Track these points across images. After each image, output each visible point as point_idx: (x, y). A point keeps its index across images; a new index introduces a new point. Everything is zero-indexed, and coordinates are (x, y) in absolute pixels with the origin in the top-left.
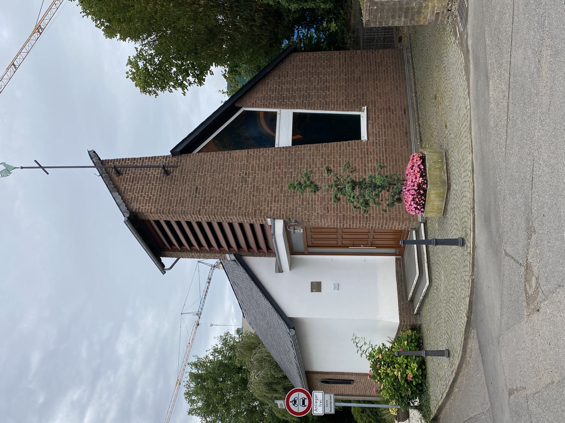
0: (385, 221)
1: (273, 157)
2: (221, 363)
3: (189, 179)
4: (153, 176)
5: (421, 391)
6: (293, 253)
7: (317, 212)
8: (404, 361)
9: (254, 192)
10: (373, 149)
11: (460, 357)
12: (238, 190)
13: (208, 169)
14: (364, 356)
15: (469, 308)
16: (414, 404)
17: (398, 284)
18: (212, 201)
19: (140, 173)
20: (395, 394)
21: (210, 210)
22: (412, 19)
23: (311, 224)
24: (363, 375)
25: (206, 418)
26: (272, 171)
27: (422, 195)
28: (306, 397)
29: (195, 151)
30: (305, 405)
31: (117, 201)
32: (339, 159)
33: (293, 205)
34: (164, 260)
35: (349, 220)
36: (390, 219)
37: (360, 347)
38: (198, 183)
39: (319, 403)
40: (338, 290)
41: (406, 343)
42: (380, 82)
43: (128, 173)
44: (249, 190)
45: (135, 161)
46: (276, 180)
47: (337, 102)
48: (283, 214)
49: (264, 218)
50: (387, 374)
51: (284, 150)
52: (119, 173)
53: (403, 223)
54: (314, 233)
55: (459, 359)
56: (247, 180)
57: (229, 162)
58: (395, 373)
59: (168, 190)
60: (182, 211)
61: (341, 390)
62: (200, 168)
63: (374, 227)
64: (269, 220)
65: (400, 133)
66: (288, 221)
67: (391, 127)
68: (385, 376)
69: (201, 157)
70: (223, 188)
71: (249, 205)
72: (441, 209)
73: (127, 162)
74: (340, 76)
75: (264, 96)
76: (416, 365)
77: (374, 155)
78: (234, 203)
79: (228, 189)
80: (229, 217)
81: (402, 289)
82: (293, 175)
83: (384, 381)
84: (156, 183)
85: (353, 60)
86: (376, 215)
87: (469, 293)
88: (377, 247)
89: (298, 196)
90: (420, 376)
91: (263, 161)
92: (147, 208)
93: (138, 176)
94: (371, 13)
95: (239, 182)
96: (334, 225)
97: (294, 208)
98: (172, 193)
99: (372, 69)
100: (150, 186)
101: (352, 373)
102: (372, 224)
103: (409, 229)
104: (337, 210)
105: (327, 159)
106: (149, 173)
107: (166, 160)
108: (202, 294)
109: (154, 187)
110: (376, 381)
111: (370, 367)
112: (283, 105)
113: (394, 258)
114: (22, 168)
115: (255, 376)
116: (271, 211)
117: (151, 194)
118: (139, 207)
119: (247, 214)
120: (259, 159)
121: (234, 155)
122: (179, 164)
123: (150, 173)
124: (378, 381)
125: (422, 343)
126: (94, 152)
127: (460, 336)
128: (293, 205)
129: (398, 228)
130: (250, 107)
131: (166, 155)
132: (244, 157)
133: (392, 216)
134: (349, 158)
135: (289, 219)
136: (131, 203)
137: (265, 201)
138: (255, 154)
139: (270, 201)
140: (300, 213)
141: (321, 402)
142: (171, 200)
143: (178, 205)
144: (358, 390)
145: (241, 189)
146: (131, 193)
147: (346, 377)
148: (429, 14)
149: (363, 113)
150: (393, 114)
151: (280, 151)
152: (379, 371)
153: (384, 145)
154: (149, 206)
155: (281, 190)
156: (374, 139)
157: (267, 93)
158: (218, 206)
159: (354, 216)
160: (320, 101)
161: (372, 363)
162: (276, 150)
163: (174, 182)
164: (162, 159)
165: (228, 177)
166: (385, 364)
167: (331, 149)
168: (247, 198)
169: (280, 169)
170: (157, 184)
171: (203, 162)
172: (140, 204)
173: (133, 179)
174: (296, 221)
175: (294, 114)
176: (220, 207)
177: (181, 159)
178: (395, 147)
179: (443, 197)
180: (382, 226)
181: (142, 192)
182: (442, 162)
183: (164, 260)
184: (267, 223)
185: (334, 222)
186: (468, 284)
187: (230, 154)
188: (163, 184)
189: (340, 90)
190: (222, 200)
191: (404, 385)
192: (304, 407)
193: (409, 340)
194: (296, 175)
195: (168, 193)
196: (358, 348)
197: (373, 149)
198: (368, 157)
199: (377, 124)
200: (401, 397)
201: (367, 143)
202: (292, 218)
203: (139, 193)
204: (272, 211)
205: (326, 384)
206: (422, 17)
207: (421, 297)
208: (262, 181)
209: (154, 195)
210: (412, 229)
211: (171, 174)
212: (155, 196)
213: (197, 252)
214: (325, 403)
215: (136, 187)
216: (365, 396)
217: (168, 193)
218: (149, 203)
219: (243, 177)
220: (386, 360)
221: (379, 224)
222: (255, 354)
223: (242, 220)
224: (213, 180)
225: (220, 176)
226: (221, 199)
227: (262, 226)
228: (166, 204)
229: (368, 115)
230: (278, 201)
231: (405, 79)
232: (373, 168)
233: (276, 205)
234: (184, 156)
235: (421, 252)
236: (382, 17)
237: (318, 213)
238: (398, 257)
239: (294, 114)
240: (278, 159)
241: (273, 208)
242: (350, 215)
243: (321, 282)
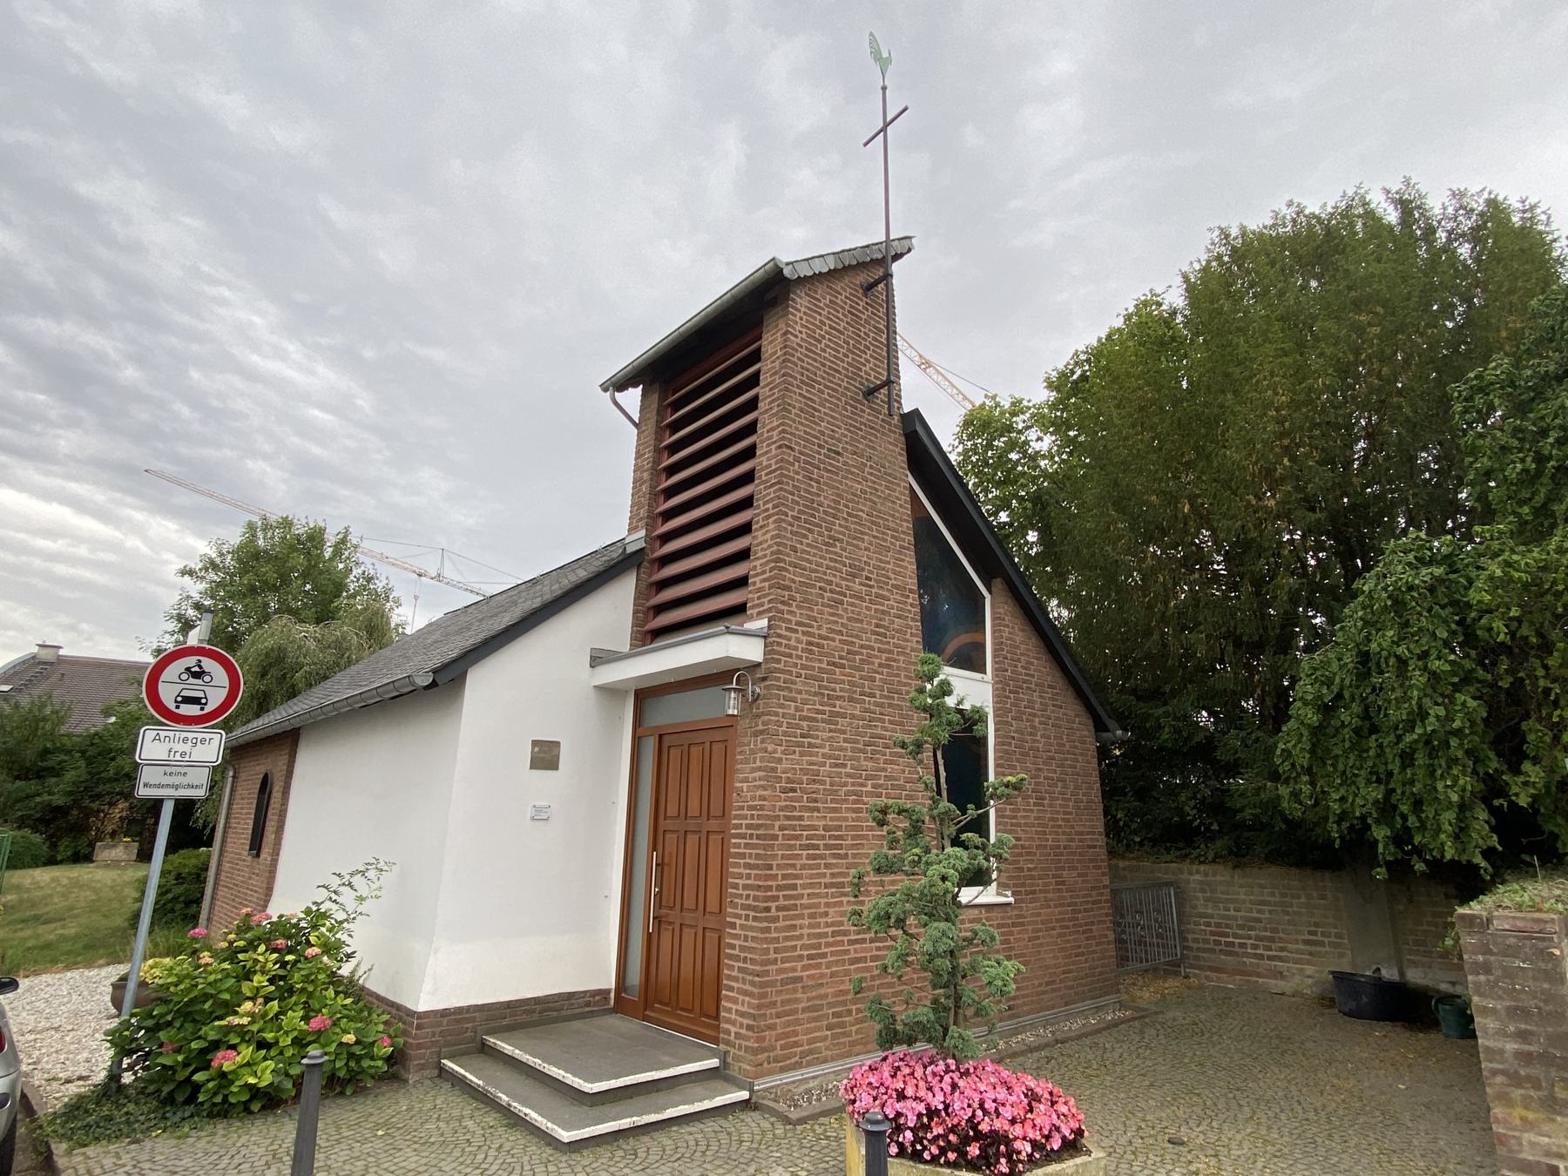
0: (758, 968)
2: (340, 587)
5: (170, 1100)
6: (640, 696)
8: (287, 1033)
12: (836, 553)
13: (876, 490)
14: (322, 895)
16: (126, 1070)
17: (536, 1000)
20: (171, 1007)
22: (1516, 1080)
23: (746, 740)
24: (268, 883)
25: (233, 553)
26: (876, 645)
27: (962, 1154)
28: (208, 709)
30: (182, 705)
33: (800, 692)
35: (763, 852)
36: (762, 985)
37: (350, 883)
39: (181, 747)
40: (533, 819)
41: (350, 1038)
42: (1060, 935)
44: (833, 579)
46: (856, 653)
48: (779, 661)
49: (769, 610)
50: (247, 975)
52: (869, 288)
53: (749, 1028)
54: (685, 753)
56: (857, 580)
57: (892, 543)
58: (248, 1006)
60: (789, 405)
61: (239, 823)
62: (880, 471)
64: (763, 623)
66: (758, 676)
68: (244, 966)
71: (802, 575)
75: (1018, 647)
76: (267, 1079)
79: (837, 528)
80: (771, 520)
81: (521, 1015)
82: (867, 699)
83: (226, 965)
86: (775, 938)
89: (821, 708)
90: (225, 1097)
94: (1525, 938)
97: (793, 695)
98: (828, 393)
99: (1080, 915)
101: (278, 855)
102: (743, 927)
104: (788, 818)
105: (904, 793)
108: (473, 585)
110: (232, 936)
111: (281, 916)
113: (610, 982)
114: (884, 89)
115: (307, 632)
116: (787, 629)
117: (826, 346)
118: (800, 311)
119: (782, 565)
120: (899, 617)
124: (231, 943)
125: (342, 1094)
126: (909, 250)
128: (800, 692)
129: (729, 1010)
130: (993, 613)
133: (769, 990)
135: (764, 679)
136: (808, 295)
137: (809, 617)
140: (780, 710)
141: (183, 754)
142: (814, 387)
144: (233, 868)
146: (828, 302)
147: (269, 837)
148: (1546, 1140)
149: (995, 893)
152: (262, 948)
155: (834, 664)
159: (771, 869)
161: (294, 921)
163: (851, 406)
165: (862, 533)
166: (284, 964)
169: (880, 665)
171: (892, 483)
173: (857, 316)
174: (756, 698)
177: (895, 432)
180: (736, 958)
184: (751, 618)
185: (751, 808)
187: (908, 549)
190: (814, 509)
191: (200, 1038)
192: (176, 701)
193: (357, 1050)
196: (348, 877)
200: (157, 1024)
202: (767, 687)
204: (787, 633)
205: (258, 786)
206: (1531, 1116)
207: (504, 1097)
209: (822, 350)
210: (724, 1057)
213: (654, 462)
214: (179, 769)
216: (216, 884)
218: (809, 336)
219: (863, 569)
220: (300, 969)
221: (742, 949)
222: (357, 634)
223: (760, 554)
224: (855, 495)
225: (864, 516)
227: (739, 610)
229: (996, 909)
231: (1067, 1004)
233: (800, 646)
235: (657, 1091)
237: (780, 761)
238: (612, 995)
240: (901, 664)
241: (793, 635)
242: (774, 857)
243: (557, 769)
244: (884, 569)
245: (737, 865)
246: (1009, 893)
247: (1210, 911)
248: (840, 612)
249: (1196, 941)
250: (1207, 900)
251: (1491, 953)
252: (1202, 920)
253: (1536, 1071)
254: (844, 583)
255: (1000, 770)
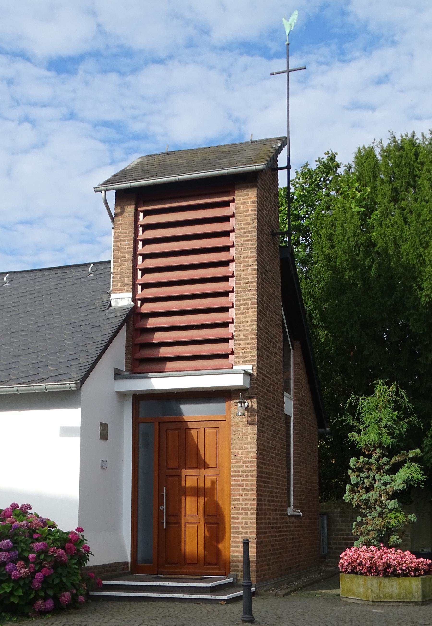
247: (344, 527)
249: (335, 544)
250: (343, 522)
252: (339, 533)
255: (296, 447)
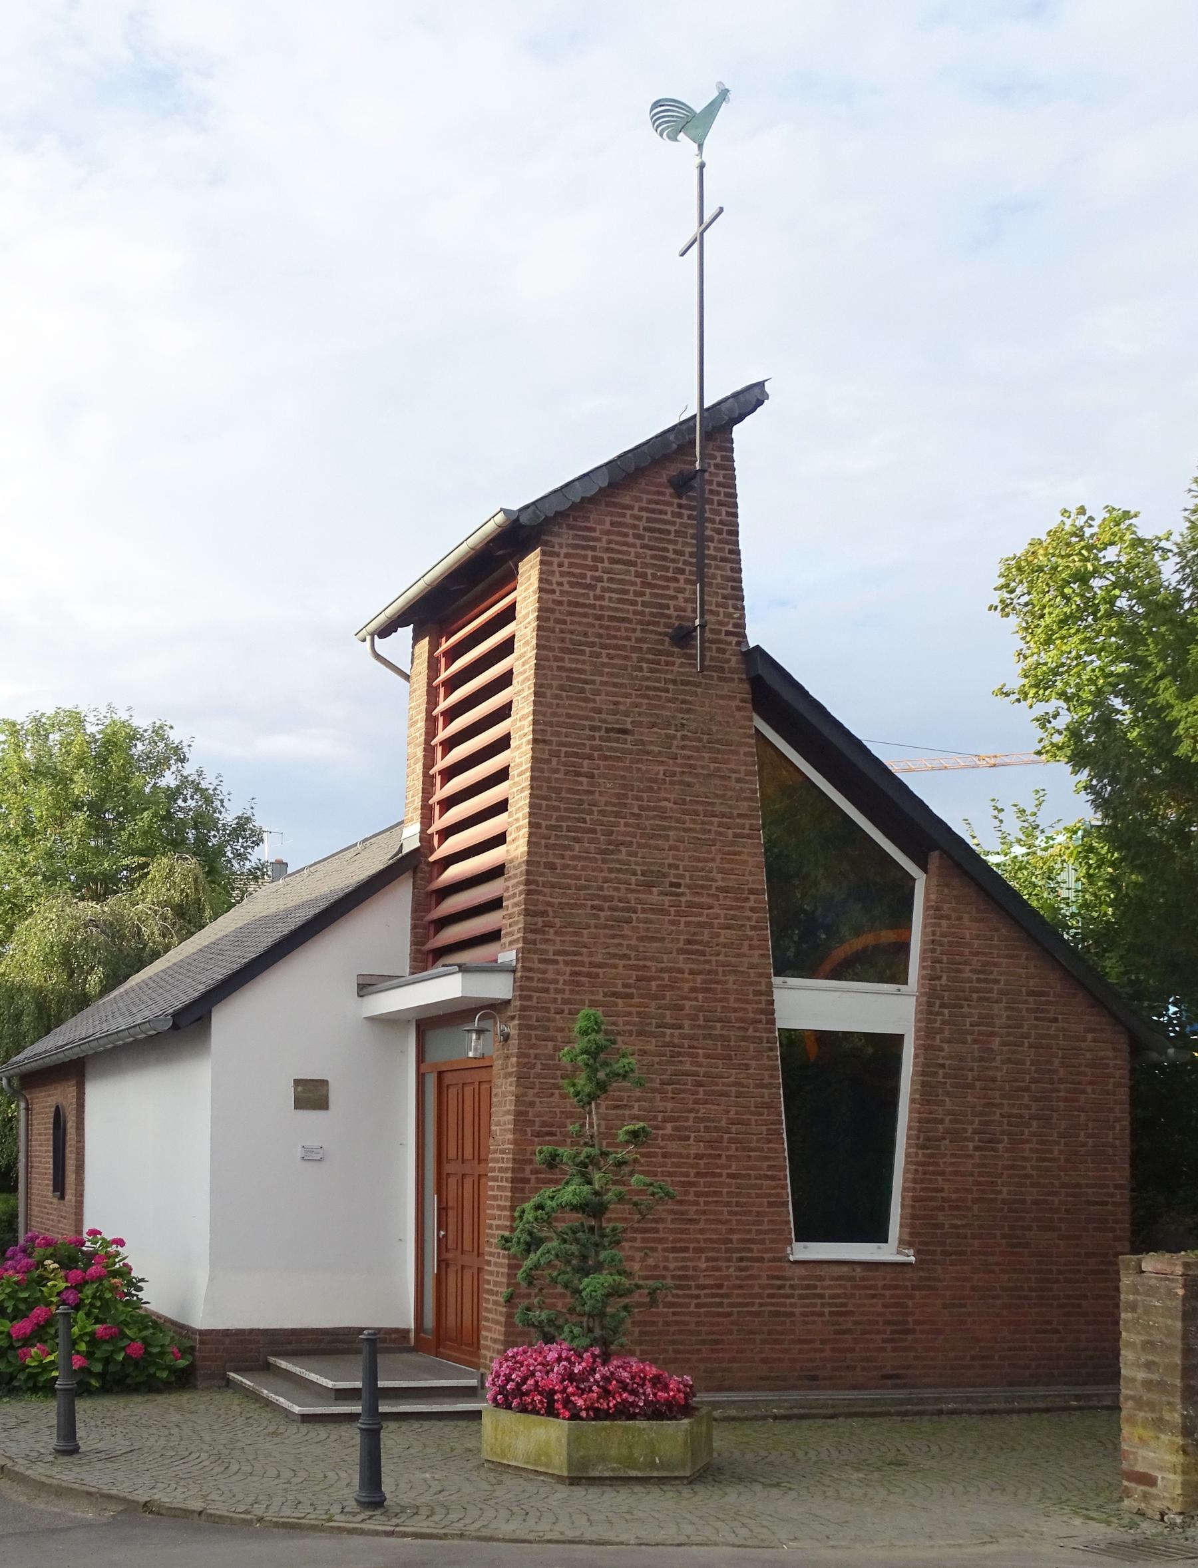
1: (734, 971)
3: (656, 707)
4: (671, 592)
6: (422, 1029)
7: (537, 1100)
9: (612, 909)
10: (758, 1277)
11: (43, 1479)
12: (619, 861)
15: (170, 1508)
18: (580, 779)
19: (682, 553)
21: (546, 775)
22: (1140, 1403)
29: (764, 723)
31: (577, 483)
32: (725, 1172)
34: (406, 632)
38: (641, 734)
43: (680, 515)
44: (615, 893)
45: (724, 535)
47: (934, 1173)
51: (763, 1006)
55: (38, 1478)
59: (621, 642)
62: (700, 740)
63: (489, 1268)
65: (811, 1360)
67: (837, 1332)
69: (740, 744)
70: (623, 815)
71: (564, 895)
72: (504, 1456)
73: (724, 509)
74: (1032, 1185)
77: (737, 1278)
78: (571, 849)
79: (622, 829)
82: (668, 1031)
84: (644, 604)
85: (1090, 1226)
87: (213, 1512)
88: (438, 1277)
91: (722, 940)
92: (554, 581)
93: (671, 547)
94: (1162, 1279)
95: (644, 864)
96: (495, 1152)
97: (551, 1033)
98: (608, 655)
99: (1055, 1286)
100: (634, 584)
101: (82, 1195)
103: (482, 1370)
105: (727, 1136)
106: (682, 581)
107: (728, 633)
109: (631, 597)
112: (930, 1004)
114: (702, 166)
116: (541, 961)
117: (604, 590)
121: (744, 847)
122: (715, 674)
123: (682, 584)
126: (760, 403)
127: (101, 1481)
131: (747, 631)
132: (735, 879)
134: (728, 1204)
137: (575, 943)
138: (749, 914)
139: (576, 958)
140: (531, 1051)
142: (582, 652)
143: (564, 674)
145: (619, 871)
146: (607, 526)
147: (71, 1177)
148: (1152, 1454)
150: (884, 1341)
151: (758, 993)
153: (772, 1308)
154: (560, 584)
155: (614, 994)
156: (796, 1282)
157: (978, 953)
158: (561, 800)
160: (942, 1121)
162: (764, 981)
164: (732, 621)
165: (664, 828)
167: (760, 1149)
168: (587, 888)
170: (639, 608)
172: (567, 556)
175: (900, 1038)
176: (557, 803)
178: (764, 1342)
179: (537, 1462)
181: (613, 561)
182: (652, 1465)
183: (406, 632)
184: (503, 947)
186: (241, 1508)
188: (639, 627)
189: (979, 1184)
194: (668, 1039)
195: (608, 641)
197: (758, 1277)
198: (729, 1260)
199: (849, 1291)
201: (780, 1260)
203: (608, 550)
204: (541, 966)
207: (265, 1392)
208: (650, 935)
211: (676, 650)
212: (598, 603)
215: (630, 540)
217: (608, 641)
218: (571, 584)
219: (664, 875)
224: (655, 781)
226: (586, 806)
228: (569, 636)
230: (578, 984)
231: (1011, 1384)
232: (691, 1273)
234: (743, 690)
236: (1148, 1311)
237: (532, 1104)
238: (412, 1335)
239: (900, 1038)
240: (730, 986)
241: (551, 967)
244: (703, 870)
245: (492, 1207)
246: (911, 1252)
248: (626, 932)
251: (1139, 1294)
253: (1153, 1396)
254: (632, 896)
